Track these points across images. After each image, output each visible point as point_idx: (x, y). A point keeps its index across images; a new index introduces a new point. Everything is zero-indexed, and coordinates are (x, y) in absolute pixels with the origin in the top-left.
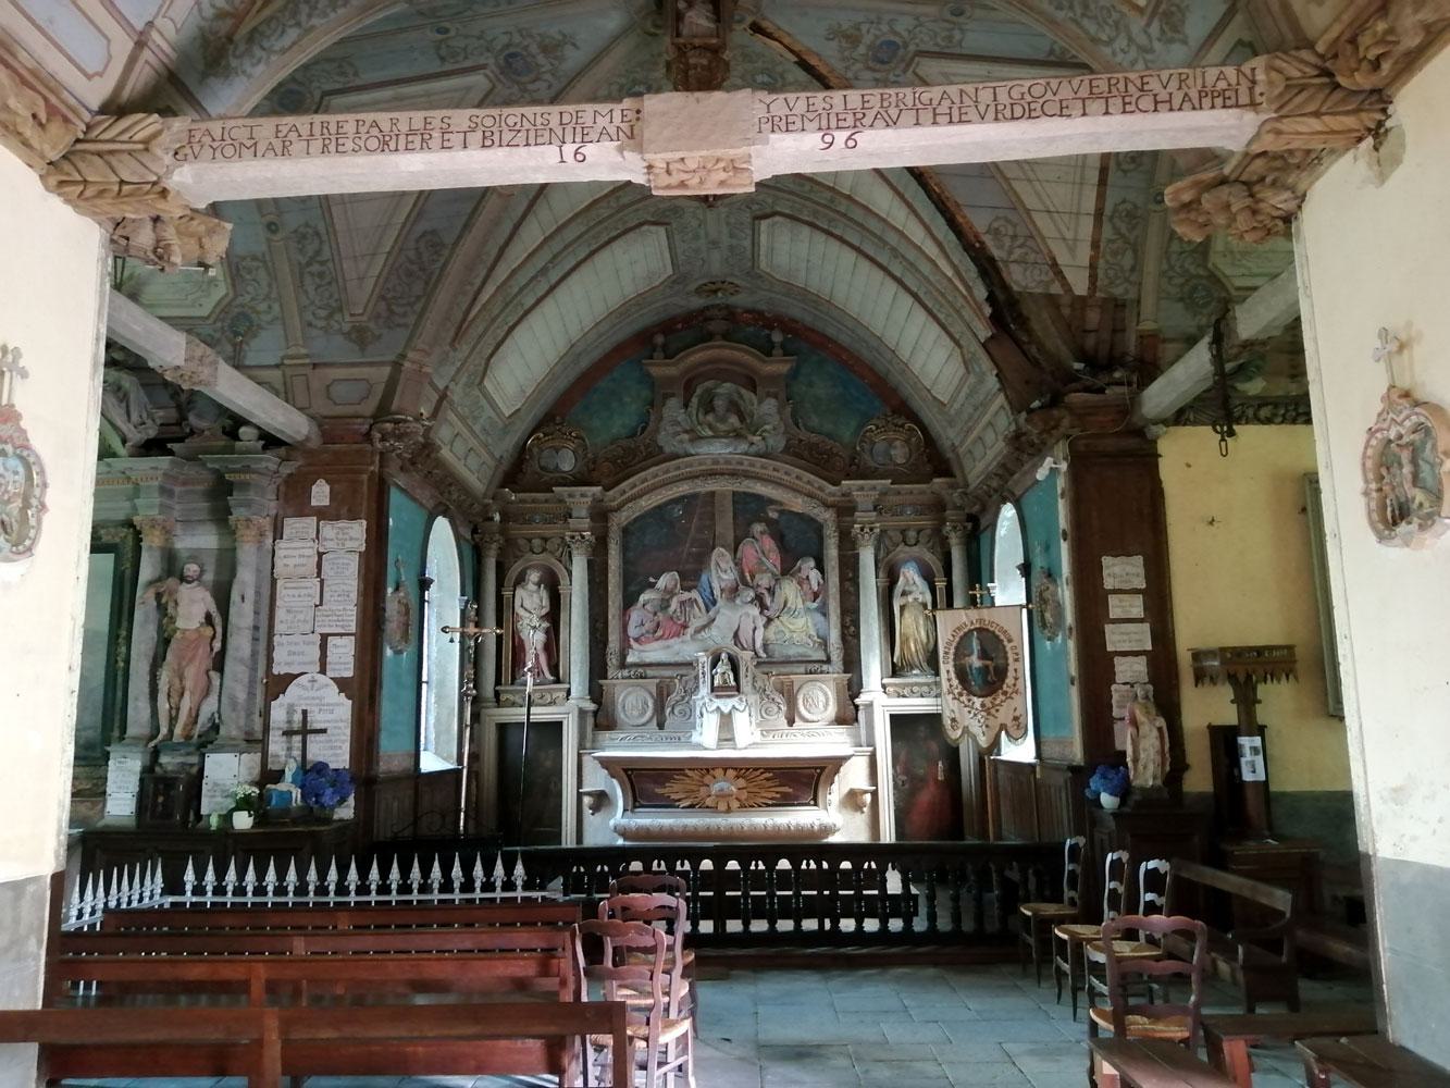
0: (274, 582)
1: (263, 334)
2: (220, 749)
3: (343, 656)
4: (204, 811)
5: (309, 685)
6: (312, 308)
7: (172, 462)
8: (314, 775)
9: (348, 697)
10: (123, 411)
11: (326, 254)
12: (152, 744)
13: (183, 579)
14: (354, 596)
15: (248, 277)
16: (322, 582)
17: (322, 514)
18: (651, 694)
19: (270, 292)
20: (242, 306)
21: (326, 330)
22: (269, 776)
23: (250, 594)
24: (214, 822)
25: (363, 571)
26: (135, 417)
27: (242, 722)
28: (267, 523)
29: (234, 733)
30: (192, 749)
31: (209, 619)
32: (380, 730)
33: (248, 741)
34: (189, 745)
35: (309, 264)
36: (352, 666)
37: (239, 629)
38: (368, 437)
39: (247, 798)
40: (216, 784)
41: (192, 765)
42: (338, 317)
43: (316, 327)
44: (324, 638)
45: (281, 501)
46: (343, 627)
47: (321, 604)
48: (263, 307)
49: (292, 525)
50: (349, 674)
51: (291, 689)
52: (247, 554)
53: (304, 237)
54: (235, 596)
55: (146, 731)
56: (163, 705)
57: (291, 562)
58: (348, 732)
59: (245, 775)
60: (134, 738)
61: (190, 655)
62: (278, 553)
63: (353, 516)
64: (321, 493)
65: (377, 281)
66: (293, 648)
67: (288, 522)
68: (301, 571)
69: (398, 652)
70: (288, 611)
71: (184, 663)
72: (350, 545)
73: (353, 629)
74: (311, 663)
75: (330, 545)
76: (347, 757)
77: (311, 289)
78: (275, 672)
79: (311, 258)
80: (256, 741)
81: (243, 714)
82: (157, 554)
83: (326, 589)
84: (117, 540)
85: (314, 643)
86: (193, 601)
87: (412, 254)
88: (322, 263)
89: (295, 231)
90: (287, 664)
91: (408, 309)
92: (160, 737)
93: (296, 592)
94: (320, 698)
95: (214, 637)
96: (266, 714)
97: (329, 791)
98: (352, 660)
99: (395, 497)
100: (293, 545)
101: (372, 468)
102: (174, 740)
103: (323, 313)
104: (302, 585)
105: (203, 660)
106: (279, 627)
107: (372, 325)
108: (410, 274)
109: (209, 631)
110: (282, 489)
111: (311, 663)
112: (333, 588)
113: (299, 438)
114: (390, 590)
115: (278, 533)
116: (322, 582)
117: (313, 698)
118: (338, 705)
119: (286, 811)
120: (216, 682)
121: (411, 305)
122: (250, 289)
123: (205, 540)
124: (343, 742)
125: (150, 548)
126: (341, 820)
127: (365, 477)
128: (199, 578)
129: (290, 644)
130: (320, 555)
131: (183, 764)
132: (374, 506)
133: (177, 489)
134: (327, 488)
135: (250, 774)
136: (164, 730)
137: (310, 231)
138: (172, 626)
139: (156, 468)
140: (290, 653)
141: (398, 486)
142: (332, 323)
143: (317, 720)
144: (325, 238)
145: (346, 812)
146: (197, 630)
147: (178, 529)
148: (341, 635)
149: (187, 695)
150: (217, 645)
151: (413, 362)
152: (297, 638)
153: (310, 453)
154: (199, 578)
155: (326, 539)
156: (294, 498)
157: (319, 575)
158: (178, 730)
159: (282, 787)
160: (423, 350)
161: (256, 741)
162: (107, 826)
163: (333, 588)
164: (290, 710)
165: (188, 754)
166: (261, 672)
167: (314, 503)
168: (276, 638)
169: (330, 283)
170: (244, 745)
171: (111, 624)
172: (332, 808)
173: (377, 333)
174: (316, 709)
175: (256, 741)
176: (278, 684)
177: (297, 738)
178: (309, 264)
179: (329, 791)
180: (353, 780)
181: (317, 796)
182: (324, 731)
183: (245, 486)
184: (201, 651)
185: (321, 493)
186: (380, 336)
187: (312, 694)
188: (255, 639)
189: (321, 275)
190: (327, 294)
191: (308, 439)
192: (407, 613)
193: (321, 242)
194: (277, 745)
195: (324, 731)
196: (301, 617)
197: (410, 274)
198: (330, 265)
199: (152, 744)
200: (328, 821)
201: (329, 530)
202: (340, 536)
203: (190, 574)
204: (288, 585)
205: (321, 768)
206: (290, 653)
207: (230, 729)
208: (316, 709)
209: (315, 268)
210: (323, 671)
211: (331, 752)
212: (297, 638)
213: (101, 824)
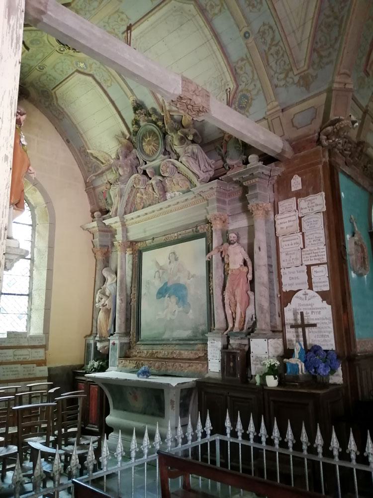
0: (277, 238)
1: (254, 102)
2: (258, 336)
3: (322, 277)
4: (253, 373)
5: (304, 297)
6: (276, 75)
7: (218, 183)
8: (312, 354)
9: (328, 303)
10: (197, 166)
11: (278, 37)
12: (226, 333)
13: (230, 243)
14: (323, 240)
15: (241, 72)
16: (303, 234)
17: (299, 195)
18: (279, 344)
19: (253, 76)
20: (242, 91)
21: (285, 86)
22: (288, 353)
23: (264, 246)
24: (258, 380)
25: (326, 224)
26: (203, 167)
27: (268, 319)
28: (269, 207)
29: (264, 327)
30: (243, 336)
31: (245, 263)
32: (353, 324)
33: (273, 331)
34: (242, 333)
35: (270, 49)
36: (328, 283)
37: (259, 266)
38: (319, 142)
39: (272, 367)
40: (257, 357)
41: (245, 345)
42: (291, 74)
43: (280, 86)
44: (309, 267)
45: (276, 193)
46: (319, 260)
47: (304, 247)
48: (251, 87)
49: (284, 205)
50: (327, 288)
51: (294, 300)
52: (260, 224)
53: (264, 33)
54: (256, 249)
55: (224, 325)
56: (229, 312)
57: (284, 226)
58: (331, 325)
59: (272, 352)
60: (218, 329)
61: (236, 283)
62: (278, 222)
63: (316, 191)
64: (296, 183)
65: (309, 40)
66: (292, 275)
67: (280, 203)
68: (291, 230)
69: (360, 275)
70: (287, 254)
71: (234, 288)
72: (316, 209)
73: (325, 260)
74: (302, 283)
75: (304, 211)
76: (333, 342)
77: (273, 64)
78: (284, 290)
79: (270, 45)
80: (279, 331)
81: (268, 316)
82: (219, 233)
83: (306, 238)
84: (205, 230)
85: (303, 271)
86: (236, 254)
87: (328, 12)
88: (276, 45)
89: (259, 31)
90: (289, 285)
91: (331, 50)
92: (229, 329)
93: (289, 243)
94: (311, 305)
95: (248, 272)
96: (282, 315)
97: (322, 366)
98: (327, 279)
99: (343, 180)
100: (285, 215)
101: (324, 160)
102: (234, 331)
103: (283, 76)
104: (292, 238)
105: (244, 286)
106: (283, 264)
107: (311, 71)
108: (329, 26)
109: (245, 269)
110: (276, 186)
111: (302, 283)
112: (310, 237)
113: (279, 151)
114: (348, 237)
115: (276, 211)
116: (303, 234)
117: (307, 305)
118: (323, 308)
119: (296, 377)
120: (252, 297)
121: (332, 46)
122: (244, 79)
123: (242, 222)
124: (329, 332)
125: (216, 230)
126: (335, 384)
127: (320, 166)
128: (238, 241)
129: (290, 273)
130: (300, 218)
131: (240, 344)
132: (328, 183)
133: (227, 200)
134: (300, 179)
135: (276, 351)
136: (231, 325)
137: (267, 27)
138: (228, 268)
139: (212, 188)
140: (291, 278)
141: (345, 173)
142: (288, 79)
143: (310, 318)
144: (275, 27)
145: (338, 378)
146: (238, 269)
147: (230, 220)
148: (318, 265)
149: (238, 305)
150: (250, 277)
151: (340, 83)
152: (293, 269)
153: (288, 162)
154: (238, 241)
155: (302, 209)
156: (282, 189)
157: (301, 230)
158: (237, 325)
159: (293, 361)
160: (344, 74)
161: (278, 331)
162: (209, 378)
163: (310, 237)
164: (295, 314)
165: (242, 338)
166: (276, 291)
167: (293, 189)
168: (282, 271)
169: (283, 56)
170: (270, 333)
171: (207, 273)
172: (327, 376)
173: (314, 74)
174: (310, 311)
175: (279, 331)
176: (287, 297)
177: (300, 330)
178: (270, 49)
179: (322, 366)
180: (338, 357)
181: (315, 368)
182: (314, 325)
183: (254, 186)
184: (242, 280)
185: (296, 183)
186: (316, 76)
187: (306, 302)
188: (270, 272)
189: (277, 53)
190: (282, 63)
191: (283, 151)
192: (363, 251)
193: (274, 32)
194: (290, 334)
195: (314, 325)
196: (294, 256)
197: (329, 26)
198: (281, 44)
199: (226, 333)
200: (325, 385)
201: (303, 203)
202: (310, 205)
203: (232, 239)
204: (285, 239)
205: (316, 349)
206: (291, 278)
207: (262, 325)
208: (310, 311)
209: (274, 49)
210: (311, 288)
211: (323, 339)
212: (293, 269)
213: (207, 376)
